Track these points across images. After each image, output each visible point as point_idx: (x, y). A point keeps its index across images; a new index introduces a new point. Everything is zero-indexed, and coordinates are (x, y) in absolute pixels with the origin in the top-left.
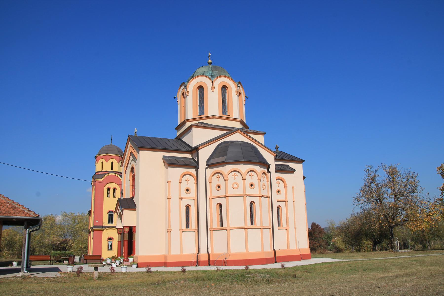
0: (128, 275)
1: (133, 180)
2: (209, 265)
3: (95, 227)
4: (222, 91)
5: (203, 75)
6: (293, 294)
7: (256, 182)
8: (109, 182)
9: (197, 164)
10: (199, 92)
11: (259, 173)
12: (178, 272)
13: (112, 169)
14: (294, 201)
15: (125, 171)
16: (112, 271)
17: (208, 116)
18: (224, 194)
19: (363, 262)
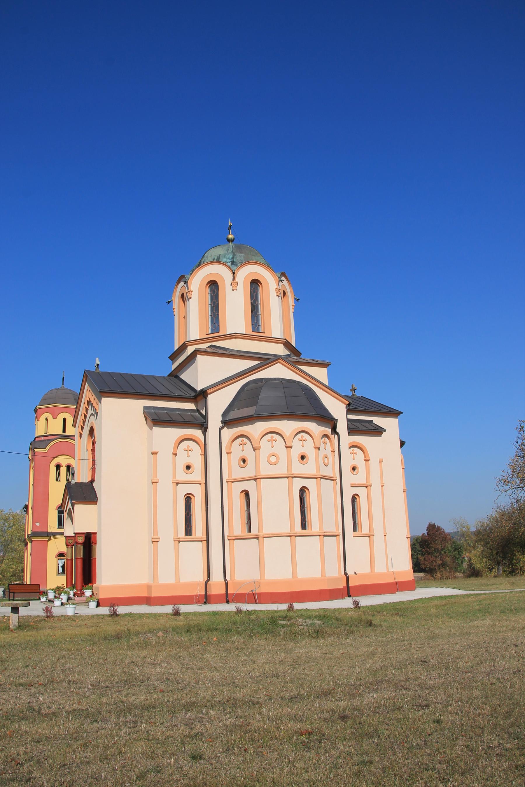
0: (75, 621)
1: (93, 451)
2: (228, 602)
3: (34, 534)
4: (251, 289)
5: (217, 261)
6: (354, 658)
7: (310, 452)
8: (59, 454)
9: (205, 421)
10: (210, 291)
11: (316, 435)
12: (167, 615)
13: (64, 431)
14: (383, 485)
15: (81, 435)
16: (47, 612)
17: (271, 337)
18: (252, 474)
19: (506, 596)
